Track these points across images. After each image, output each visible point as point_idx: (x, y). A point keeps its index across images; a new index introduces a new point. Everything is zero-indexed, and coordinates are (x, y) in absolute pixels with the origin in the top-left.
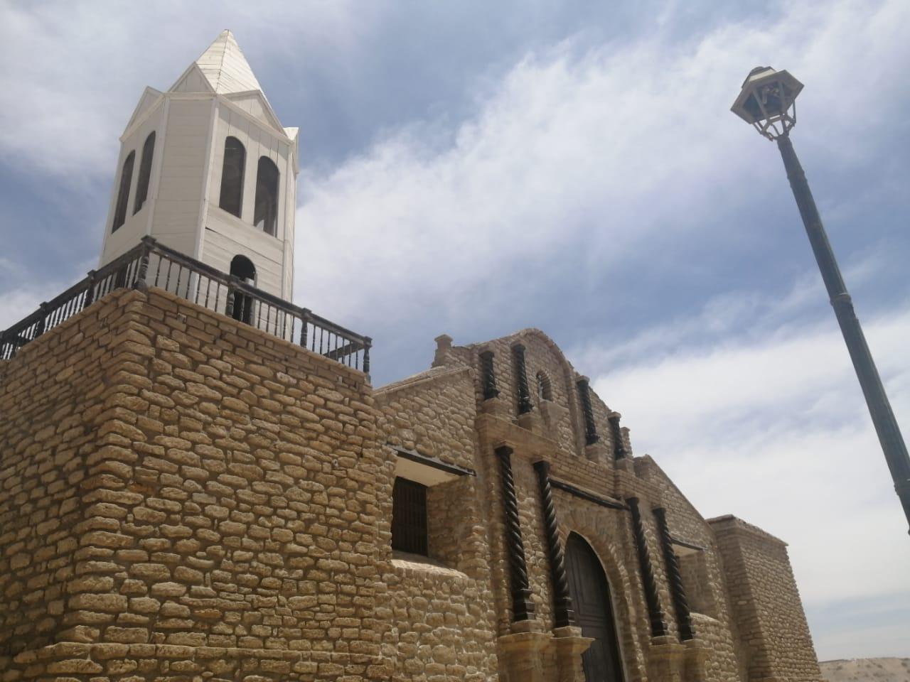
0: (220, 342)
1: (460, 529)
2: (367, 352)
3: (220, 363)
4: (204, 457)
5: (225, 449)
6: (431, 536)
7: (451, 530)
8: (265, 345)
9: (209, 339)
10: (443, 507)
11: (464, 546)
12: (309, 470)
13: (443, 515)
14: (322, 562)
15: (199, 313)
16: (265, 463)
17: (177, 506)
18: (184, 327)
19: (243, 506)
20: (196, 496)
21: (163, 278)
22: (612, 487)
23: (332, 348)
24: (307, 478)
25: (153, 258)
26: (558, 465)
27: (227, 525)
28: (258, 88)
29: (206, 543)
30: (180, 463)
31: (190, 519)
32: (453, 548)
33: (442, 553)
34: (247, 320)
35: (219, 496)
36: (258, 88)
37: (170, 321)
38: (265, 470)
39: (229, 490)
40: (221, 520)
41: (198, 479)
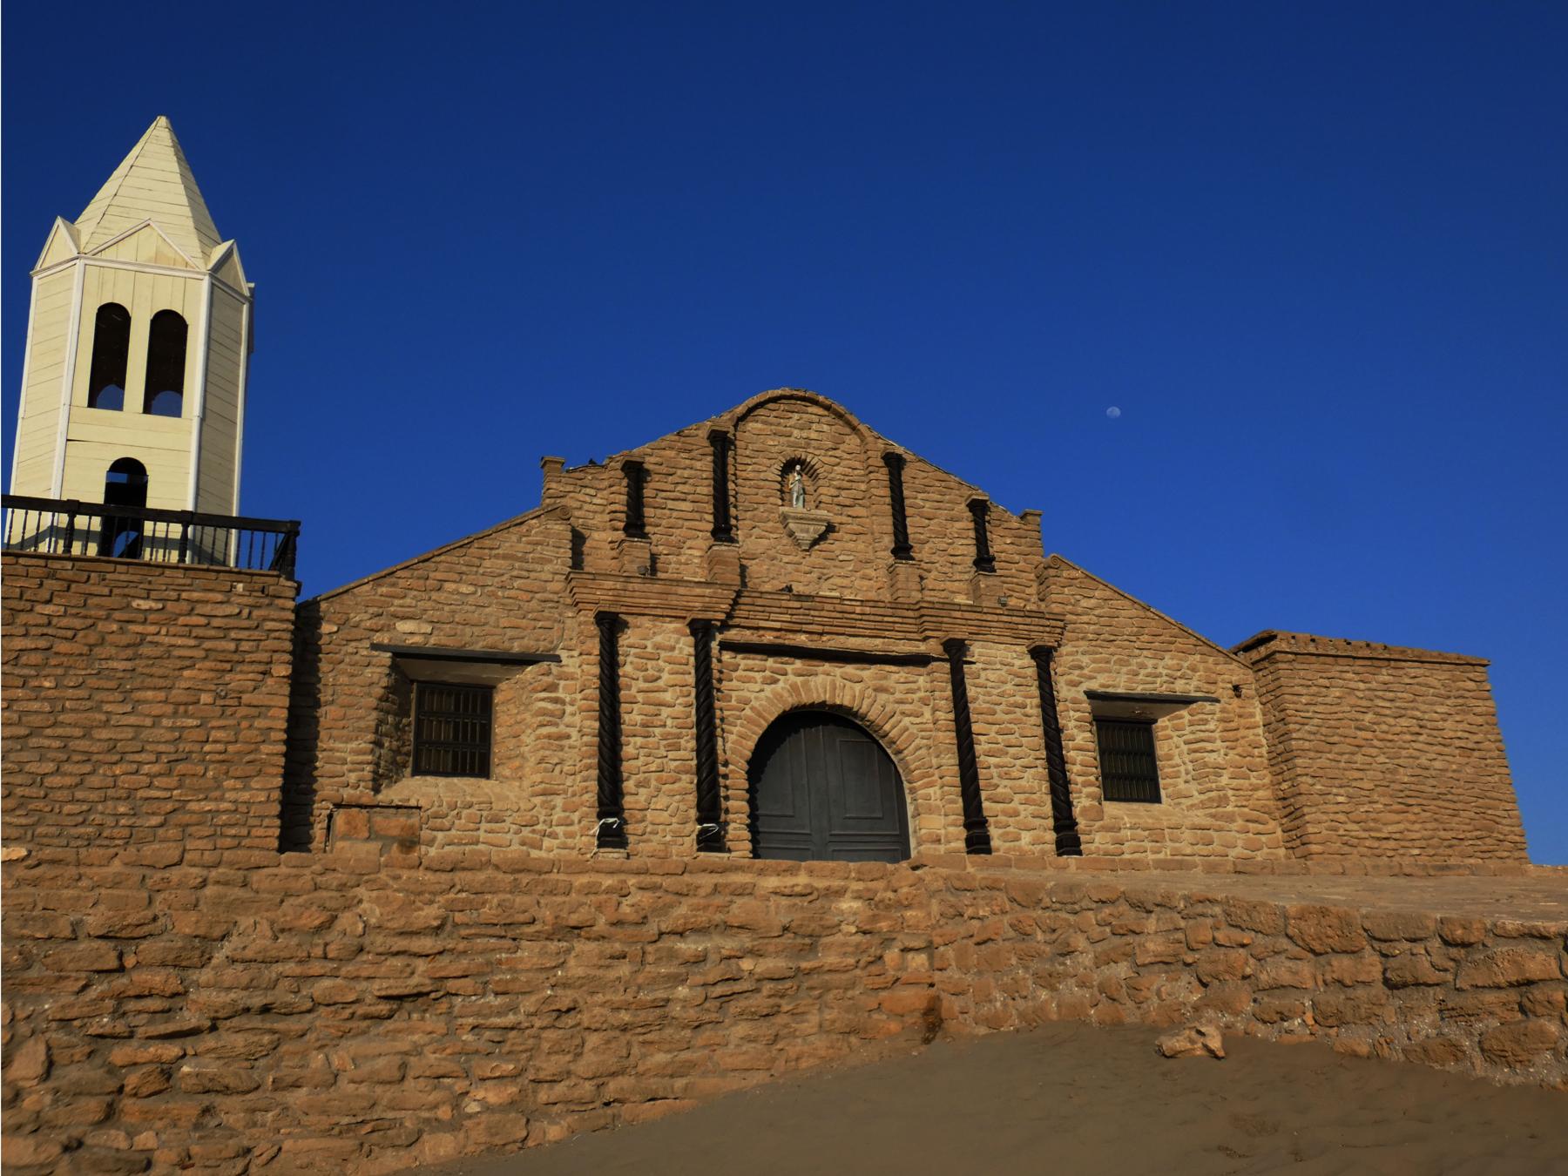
0: (47, 583)
19: (76, 758)
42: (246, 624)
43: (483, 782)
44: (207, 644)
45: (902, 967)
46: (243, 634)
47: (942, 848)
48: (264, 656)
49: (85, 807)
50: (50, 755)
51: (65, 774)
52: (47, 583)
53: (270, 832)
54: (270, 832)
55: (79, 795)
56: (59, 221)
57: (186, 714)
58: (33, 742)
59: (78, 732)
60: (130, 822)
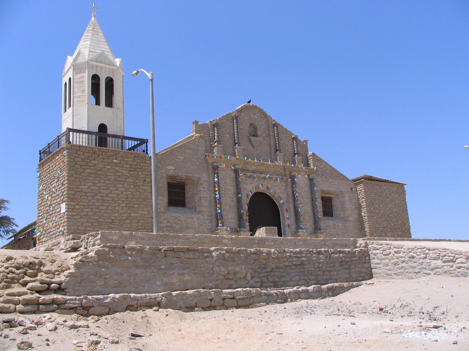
0: (94, 155)
1: (197, 198)
2: (147, 145)
3: (94, 162)
4: (92, 190)
5: (98, 186)
6: (187, 200)
7: (194, 198)
8: (108, 152)
9: (90, 155)
10: (191, 190)
11: (198, 203)
12: (126, 188)
13: (191, 193)
14: (132, 215)
15: (86, 147)
16: (111, 188)
17: (86, 204)
18: (82, 153)
19: (105, 202)
20: (91, 201)
21: (78, 140)
22: (283, 171)
23: (130, 147)
24: (125, 191)
25: (71, 133)
26: (250, 167)
27: (101, 208)
28: (77, 62)
29: (96, 213)
30: (86, 193)
31: (90, 207)
32: (194, 204)
33: (191, 206)
34: (105, 145)
35: (98, 200)
36: (77, 62)
37: (78, 152)
38: (111, 190)
39: (101, 198)
40: (99, 206)
41: (91, 196)
42: (139, 167)
43: (111, 108)
44: (131, 172)
45: (365, 259)
46: (139, 170)
47: (364, 204)
48: (144, 176)
49: (109, 215)
50: (100, 201)
51: (103, 206)
52: (94, 155)
53: (81, 136)
54: (81, 136)
55: (107, 211)
56: (68, 57)
57: (128, 191)
58: (96, 197)
59: (105, 195)
60: (138, 246)
